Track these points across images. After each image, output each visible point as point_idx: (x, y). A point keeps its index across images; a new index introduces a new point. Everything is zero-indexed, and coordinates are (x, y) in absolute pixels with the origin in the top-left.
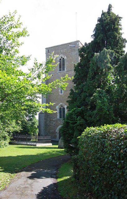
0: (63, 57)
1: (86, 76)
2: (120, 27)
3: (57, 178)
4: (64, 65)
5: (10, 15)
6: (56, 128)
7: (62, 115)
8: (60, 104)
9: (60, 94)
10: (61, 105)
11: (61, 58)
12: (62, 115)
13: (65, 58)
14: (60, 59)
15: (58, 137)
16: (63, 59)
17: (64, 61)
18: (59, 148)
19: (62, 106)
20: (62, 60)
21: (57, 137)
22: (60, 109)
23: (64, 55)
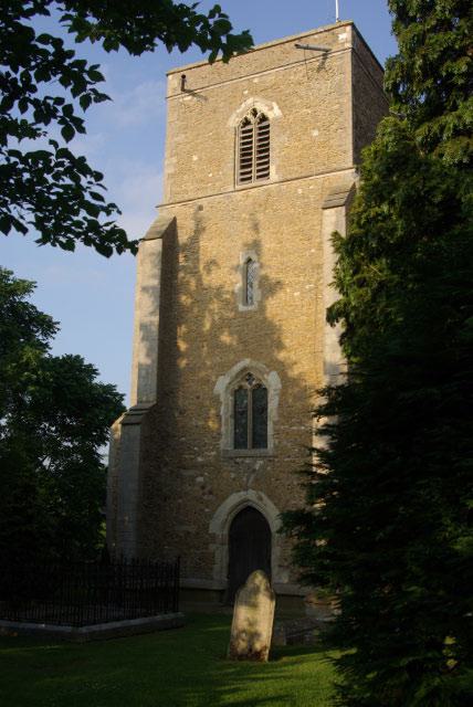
0: (262, 108)
1: (353, 201)
2: (220, 56)
3: (90, 215)
4: (264, 149)
5: (333, 697)
6: (214, 511)
7: (249, 431)
8: (237, 368)
9: (241, 308)
10: (245, 369)
11: (250, 117)
12: (249, 431)
13: (274, 113)
14: (247, 122)
15: (226, 560)
16: (264, 118)
17: (264, 133)
18: (222, 693)
19: (249, 377)
20: (254, 126)
21: (217, 567)
22: (238, 393)
23: (266, 97)
